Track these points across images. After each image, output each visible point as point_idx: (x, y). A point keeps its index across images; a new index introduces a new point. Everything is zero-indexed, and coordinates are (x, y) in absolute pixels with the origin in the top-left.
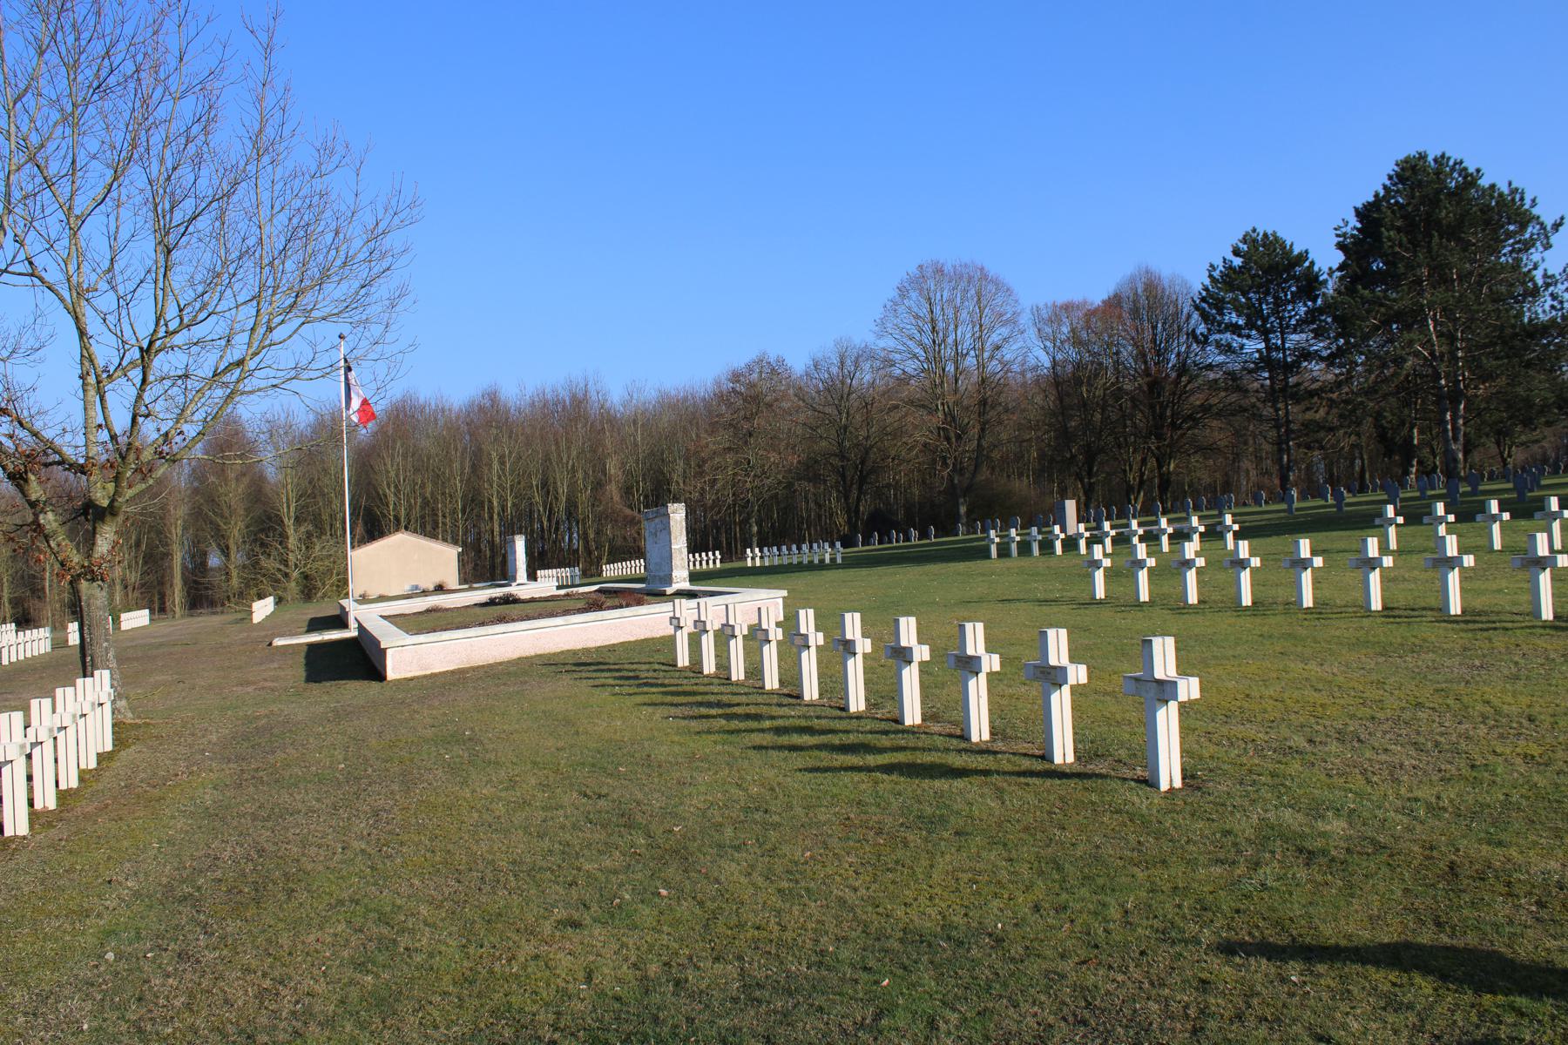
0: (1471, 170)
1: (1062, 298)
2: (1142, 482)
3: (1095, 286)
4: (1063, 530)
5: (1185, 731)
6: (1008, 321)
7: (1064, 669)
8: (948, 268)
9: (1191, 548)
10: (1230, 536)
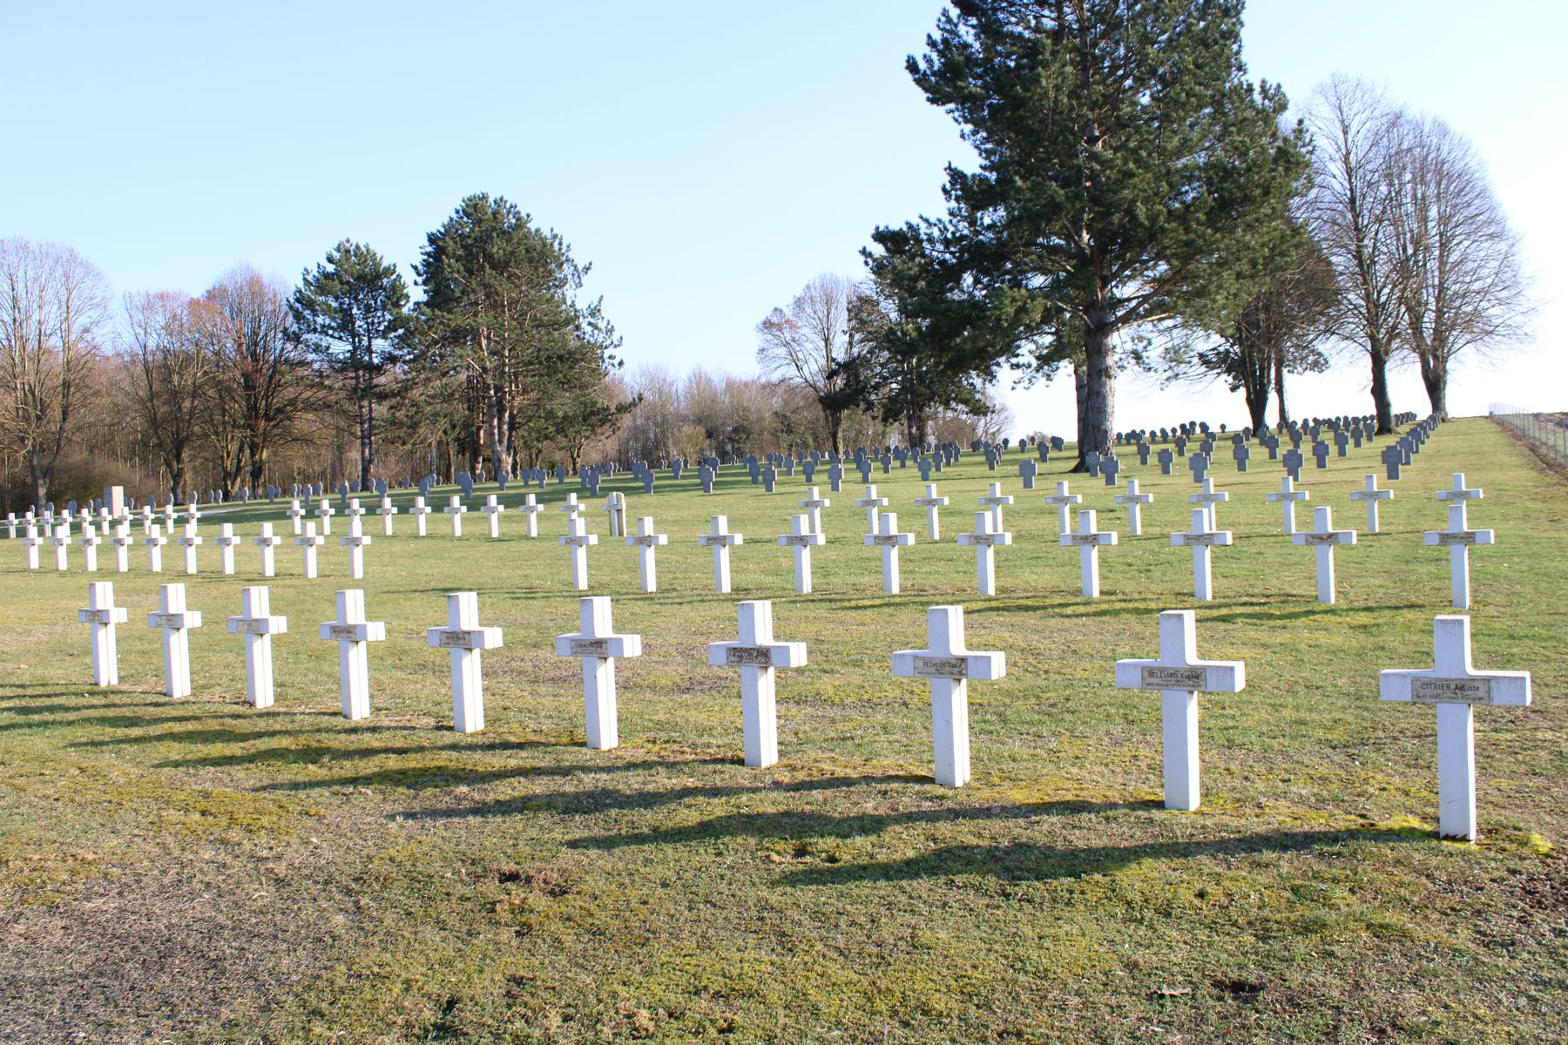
0: (523, 214)
1: (156, 288)
2: (239, 469)
3: (193, 282)
4: (111, 512)
5: (372, 668)
6: (98, 305)
7: (266, 620)
8: (33, 245)
9: (192, 529)
10: (297, 520)
